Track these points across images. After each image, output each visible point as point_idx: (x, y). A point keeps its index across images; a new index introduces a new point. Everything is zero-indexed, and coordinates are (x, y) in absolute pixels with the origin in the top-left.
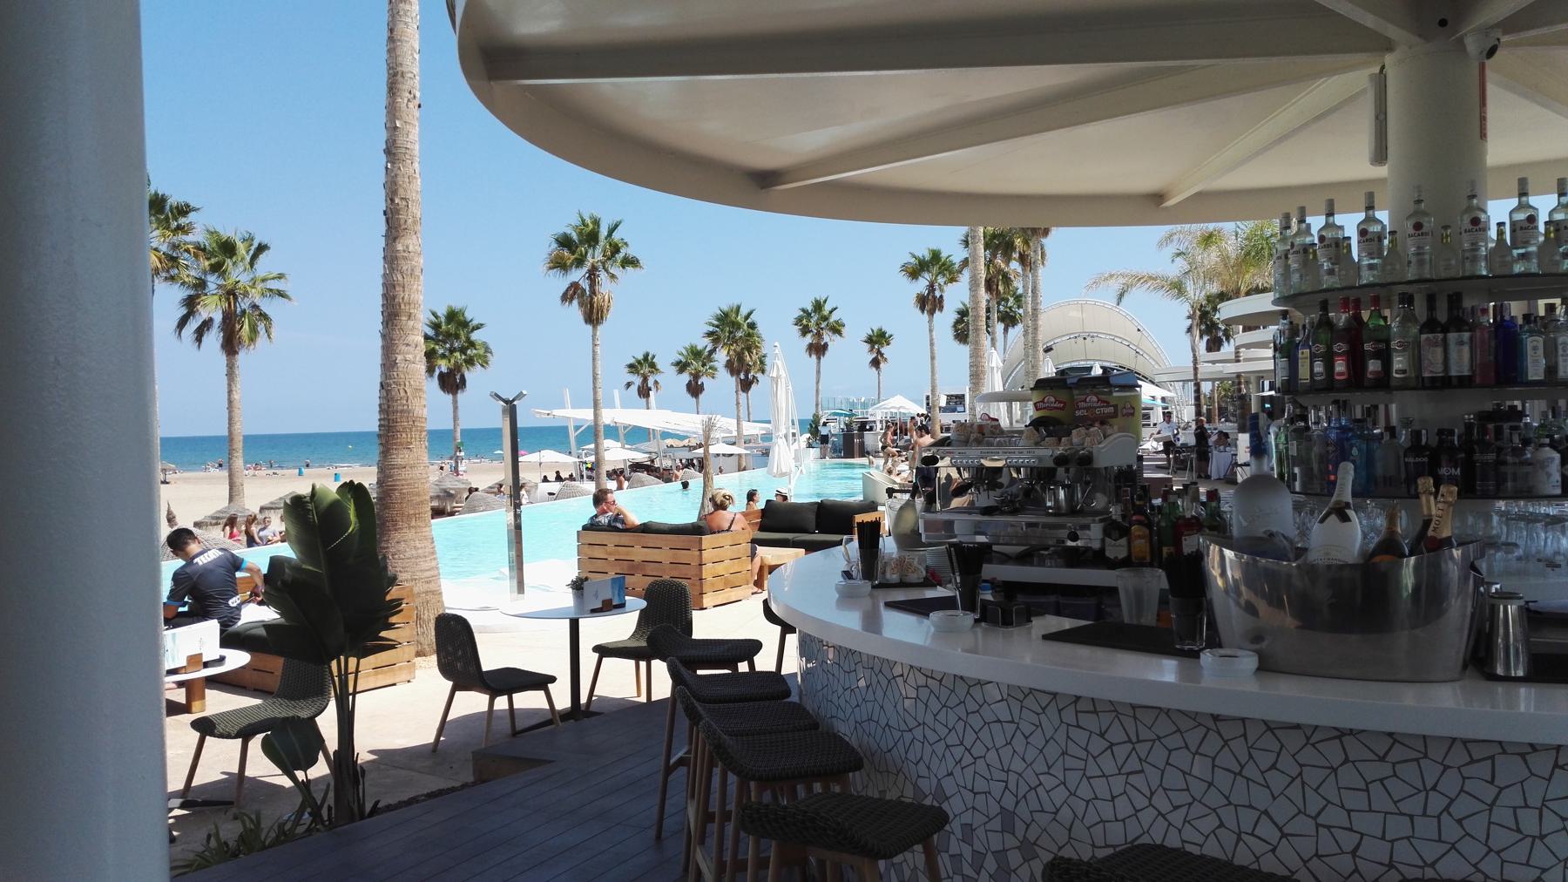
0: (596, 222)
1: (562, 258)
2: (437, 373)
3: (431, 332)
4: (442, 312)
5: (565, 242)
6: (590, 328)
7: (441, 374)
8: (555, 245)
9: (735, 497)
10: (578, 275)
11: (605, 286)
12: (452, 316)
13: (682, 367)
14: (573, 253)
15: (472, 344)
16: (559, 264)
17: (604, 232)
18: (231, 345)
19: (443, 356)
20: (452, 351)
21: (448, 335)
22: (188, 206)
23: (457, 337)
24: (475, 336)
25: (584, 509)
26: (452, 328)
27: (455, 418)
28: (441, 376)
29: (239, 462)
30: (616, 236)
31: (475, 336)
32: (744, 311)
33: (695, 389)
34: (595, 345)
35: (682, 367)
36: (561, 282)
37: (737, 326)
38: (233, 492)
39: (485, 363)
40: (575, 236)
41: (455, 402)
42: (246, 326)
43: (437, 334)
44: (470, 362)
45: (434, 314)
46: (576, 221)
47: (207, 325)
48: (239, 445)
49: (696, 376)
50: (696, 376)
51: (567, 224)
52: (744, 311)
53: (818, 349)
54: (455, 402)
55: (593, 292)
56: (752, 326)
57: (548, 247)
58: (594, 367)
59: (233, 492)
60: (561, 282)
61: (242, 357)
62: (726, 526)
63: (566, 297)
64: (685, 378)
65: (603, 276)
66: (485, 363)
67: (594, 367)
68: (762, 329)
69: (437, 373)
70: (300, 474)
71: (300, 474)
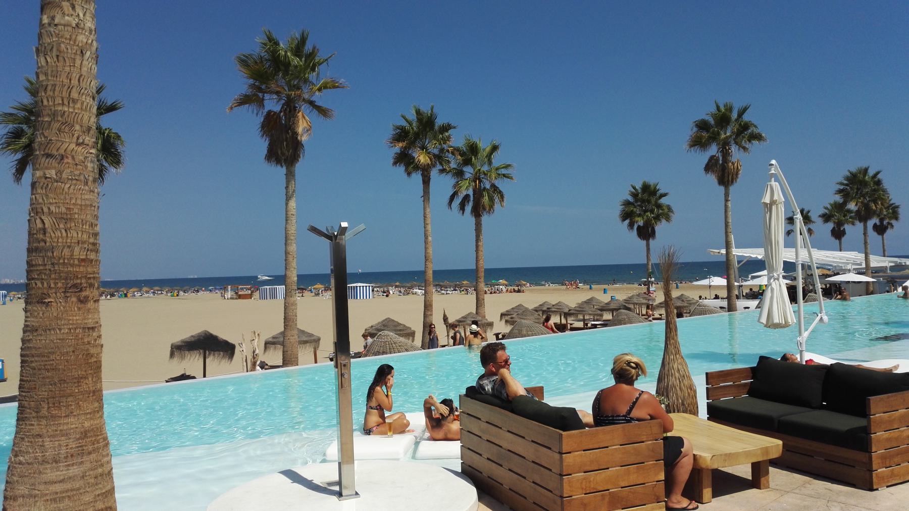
0: (730, 109)
1: (701, 138)
2: (636, 227)
3: (631, 199)
4: (639, 186)
5: (702, 126)
6: (722, 188)
7: (639, 227)
8: (695, 129)
9: (647, 366)
10: (713, 150)
11: (736, 153)
12: (646, 187)
13: (826, 218)
14: (708, 131)
15: (659, 206)
16: (698, 143)
17: (734, 115)
18: (477, 212)
19: (639, 215)
20: (645, 211)
21: (643, 201)
22: (449, 125)
23: (649, 202)
24: (663, 201)
25: (467, 368)
26: (646, 196)
27: (477, 260)
28: (639, 228)
29: (482, 286)
30: (746, 117)
31: (663, 201)
32: (871, 172)
33: (838, 234)
34: (727, 200)
35: (826, 218)
36: (703, 157)
37: (864, 183)
38: (479, 303)
39: (668, 219)
40: (712, 122)
41: (648, 245)
42: (487, 198)
43: (636, 201)
44: (658, 218)
45: (634, 188)
46: (713, 109)
47: (467, 197)
48: (482, 274)
49: (839, 224)
50: (839, 224)
51: (706, 112)
52: (871, 172)
53: (724, 173)
54: (648, 245)
55: (725, 160)
56: (879, 183)
57: (688, 131)
58: (726, 217)
59: (479, 303)
60: (703, 157)
61: (485, 219)
62: (623, 410)
63: (708, 168)
64: (830, 225)
65: (734, 149)
66: (668, 219)
67: (726, 217)
68: (886, 184)
69: (636, 227)
70: (591, 288)
71: (591, 288)
